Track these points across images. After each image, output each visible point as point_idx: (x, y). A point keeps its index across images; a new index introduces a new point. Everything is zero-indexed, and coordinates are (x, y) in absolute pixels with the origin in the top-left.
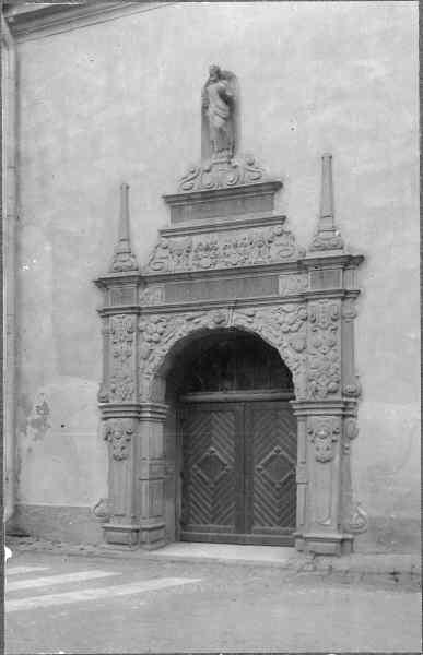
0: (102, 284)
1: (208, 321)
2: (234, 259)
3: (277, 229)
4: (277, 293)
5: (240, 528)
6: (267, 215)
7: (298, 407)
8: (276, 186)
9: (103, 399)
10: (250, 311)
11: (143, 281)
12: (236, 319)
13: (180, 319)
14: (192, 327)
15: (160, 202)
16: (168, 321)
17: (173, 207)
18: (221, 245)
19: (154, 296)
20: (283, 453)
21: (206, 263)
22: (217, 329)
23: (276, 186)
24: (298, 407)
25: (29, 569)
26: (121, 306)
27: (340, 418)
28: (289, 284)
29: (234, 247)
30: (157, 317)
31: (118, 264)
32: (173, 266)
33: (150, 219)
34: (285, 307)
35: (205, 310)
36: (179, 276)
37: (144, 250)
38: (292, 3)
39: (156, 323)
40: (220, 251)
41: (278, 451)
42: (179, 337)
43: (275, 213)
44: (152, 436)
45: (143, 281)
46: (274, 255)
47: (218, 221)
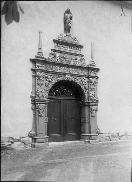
31: (38, 56)
37: (46, 55)
42: (57, 81)
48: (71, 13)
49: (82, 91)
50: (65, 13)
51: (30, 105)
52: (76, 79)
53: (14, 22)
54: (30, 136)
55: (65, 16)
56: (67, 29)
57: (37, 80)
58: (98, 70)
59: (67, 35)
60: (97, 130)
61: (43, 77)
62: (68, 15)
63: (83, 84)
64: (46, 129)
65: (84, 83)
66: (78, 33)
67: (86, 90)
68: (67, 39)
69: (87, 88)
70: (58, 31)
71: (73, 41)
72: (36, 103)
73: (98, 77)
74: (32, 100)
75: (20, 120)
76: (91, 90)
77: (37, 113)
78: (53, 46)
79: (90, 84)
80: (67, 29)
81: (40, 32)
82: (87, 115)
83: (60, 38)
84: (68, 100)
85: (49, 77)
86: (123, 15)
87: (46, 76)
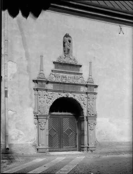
0: (35, 81)
1: (64, 95)
2: (71, 81)
3: (80, 76)
4: (80, 91)
5: (60, 147)
6: (77, 72)
7: (39, 116)
8: (81, 66)
9: (35, 113)
10: (74, 94)
11: (48, 82)
12: (71, 95)
13: (57, 93)
14: (60, 96)
15: (53, 63)
16: (54, 94)
17: (55, 65)
18: (67, 77)
19: (50, 86)
20: (70, 128)
21: (64, 81)
22: (66, 97)
23: (81, 66)
24: (39, 116)
25: (121, 156)
26: (41, 88)
27: (37, 119)
28: (83, 89)
29: (70, 78)
30: (52, 92)
31: (40, 77)
32: (54, 79)
33: (48, 68)
34: (82, 94)
35: (64, 92)
36: (58, 83)
37: (47, 74)
38: (131, 38)
39: (51, 94)
40: (67, 78)
41: (69, 128)
42: (57, 98)
43: (80, 72)
44: (46, 124)
45: (48, 82)
46: (79, 82)
47: (67, 71)
48: (70, 37)
49: (80, 106)
50: (65, 36)
51: (62, 45)
52: (75, 95)
53: (31, 17)
54: (34, 146)
55: (64, 40)
56: (67, 51)
57: (39, 98)
58: (96, 86)
59: (66, 57)
60: (95, 142)
61: (45, 96)
62: (67, 39)
63: (82, 100)
64: (99, 21)
65: (82, 99)
66: (78, 54)
67: (84, 106)
68: (67, 60)
69: (86, 103)
70: (57, 53)
71: (70, 62)
72: (38, 118)
73: (97, 93)
74: (35, 116)
75: (25, 130)
76: (89, 105)
77: (39, 126)
78: (53, 67)
79: (88, 99)
80: (67, 51)
81: (42, 56)
82: (86, 129)
83: (59, 60)
84: (66, 117)
85: (50, 95)
86: (121, 33)
87: (47, 94)
